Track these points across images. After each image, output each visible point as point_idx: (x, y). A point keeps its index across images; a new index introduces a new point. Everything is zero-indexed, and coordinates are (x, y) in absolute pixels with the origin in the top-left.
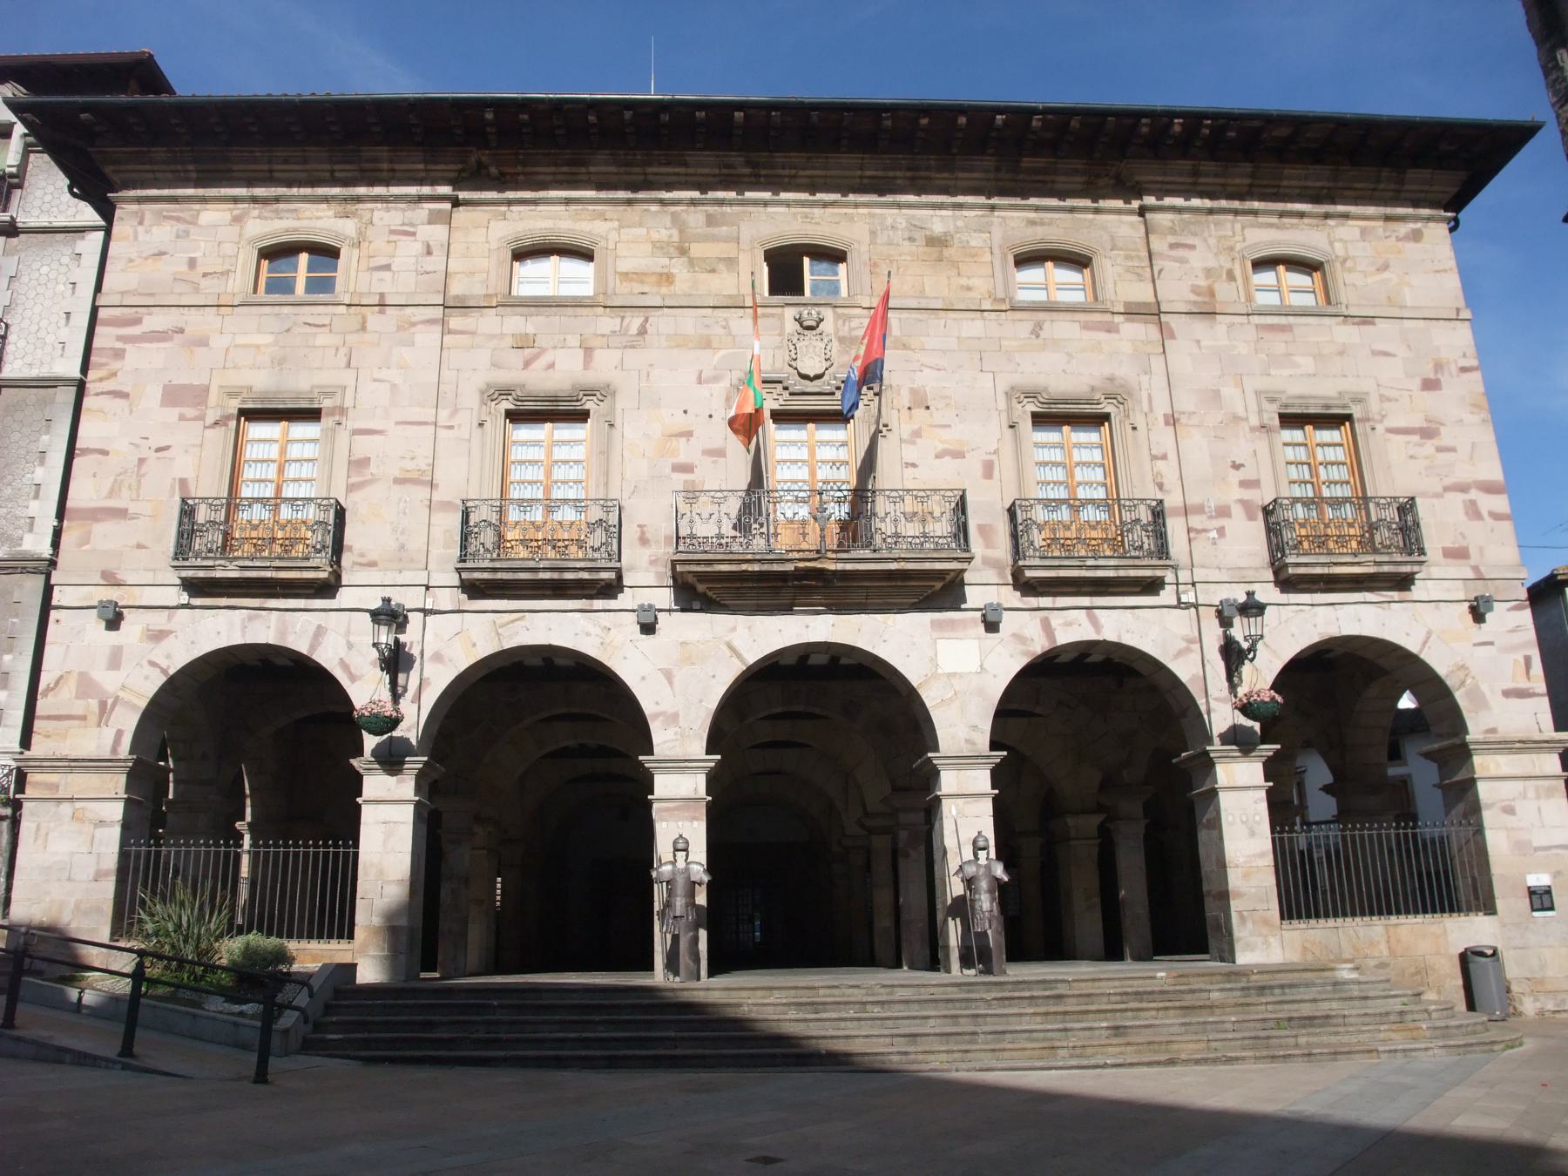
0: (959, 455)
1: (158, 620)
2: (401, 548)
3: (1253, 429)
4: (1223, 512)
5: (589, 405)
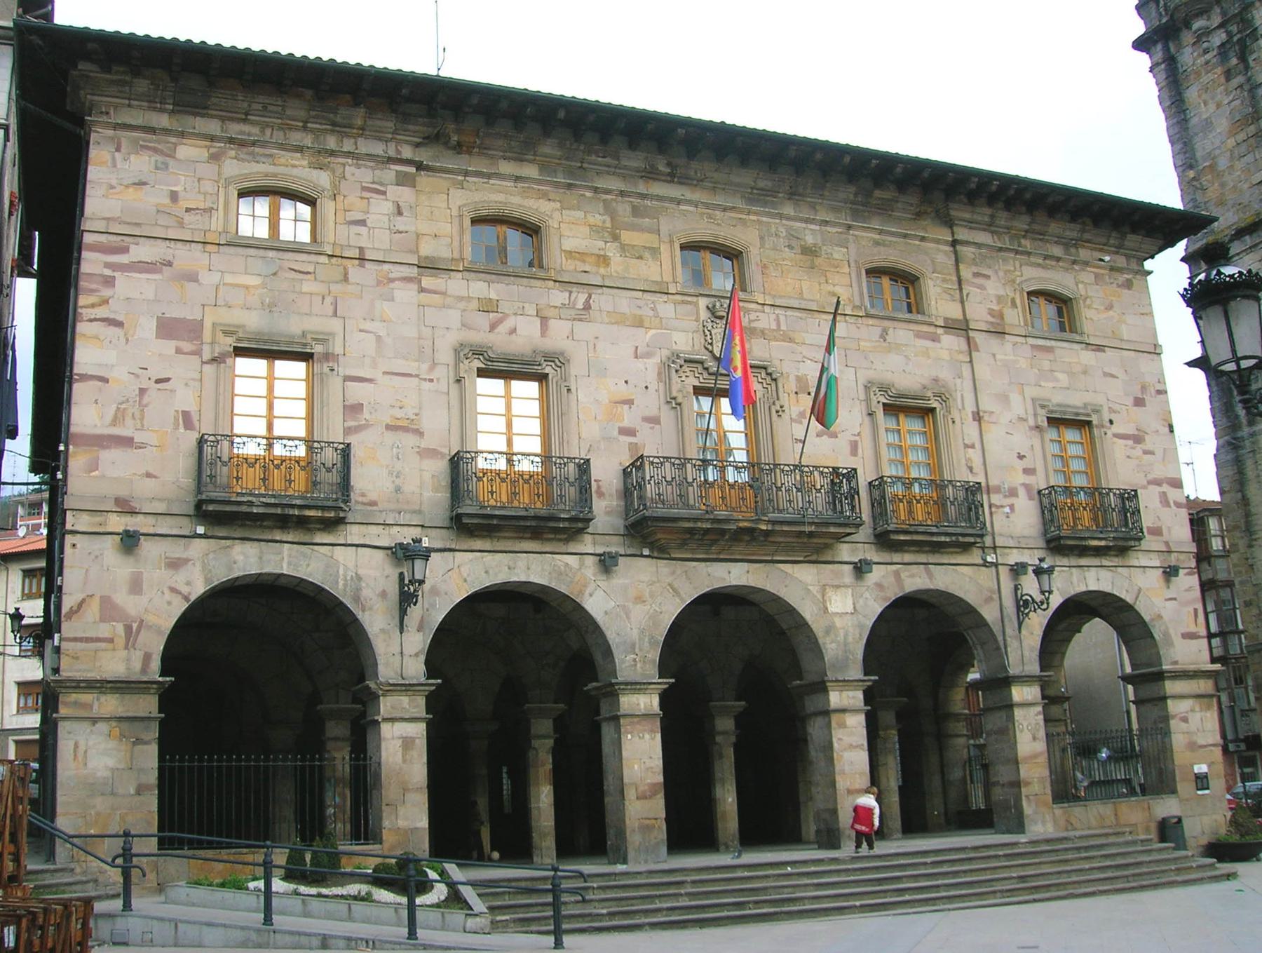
1: (175, 550)
2: (395, 478)
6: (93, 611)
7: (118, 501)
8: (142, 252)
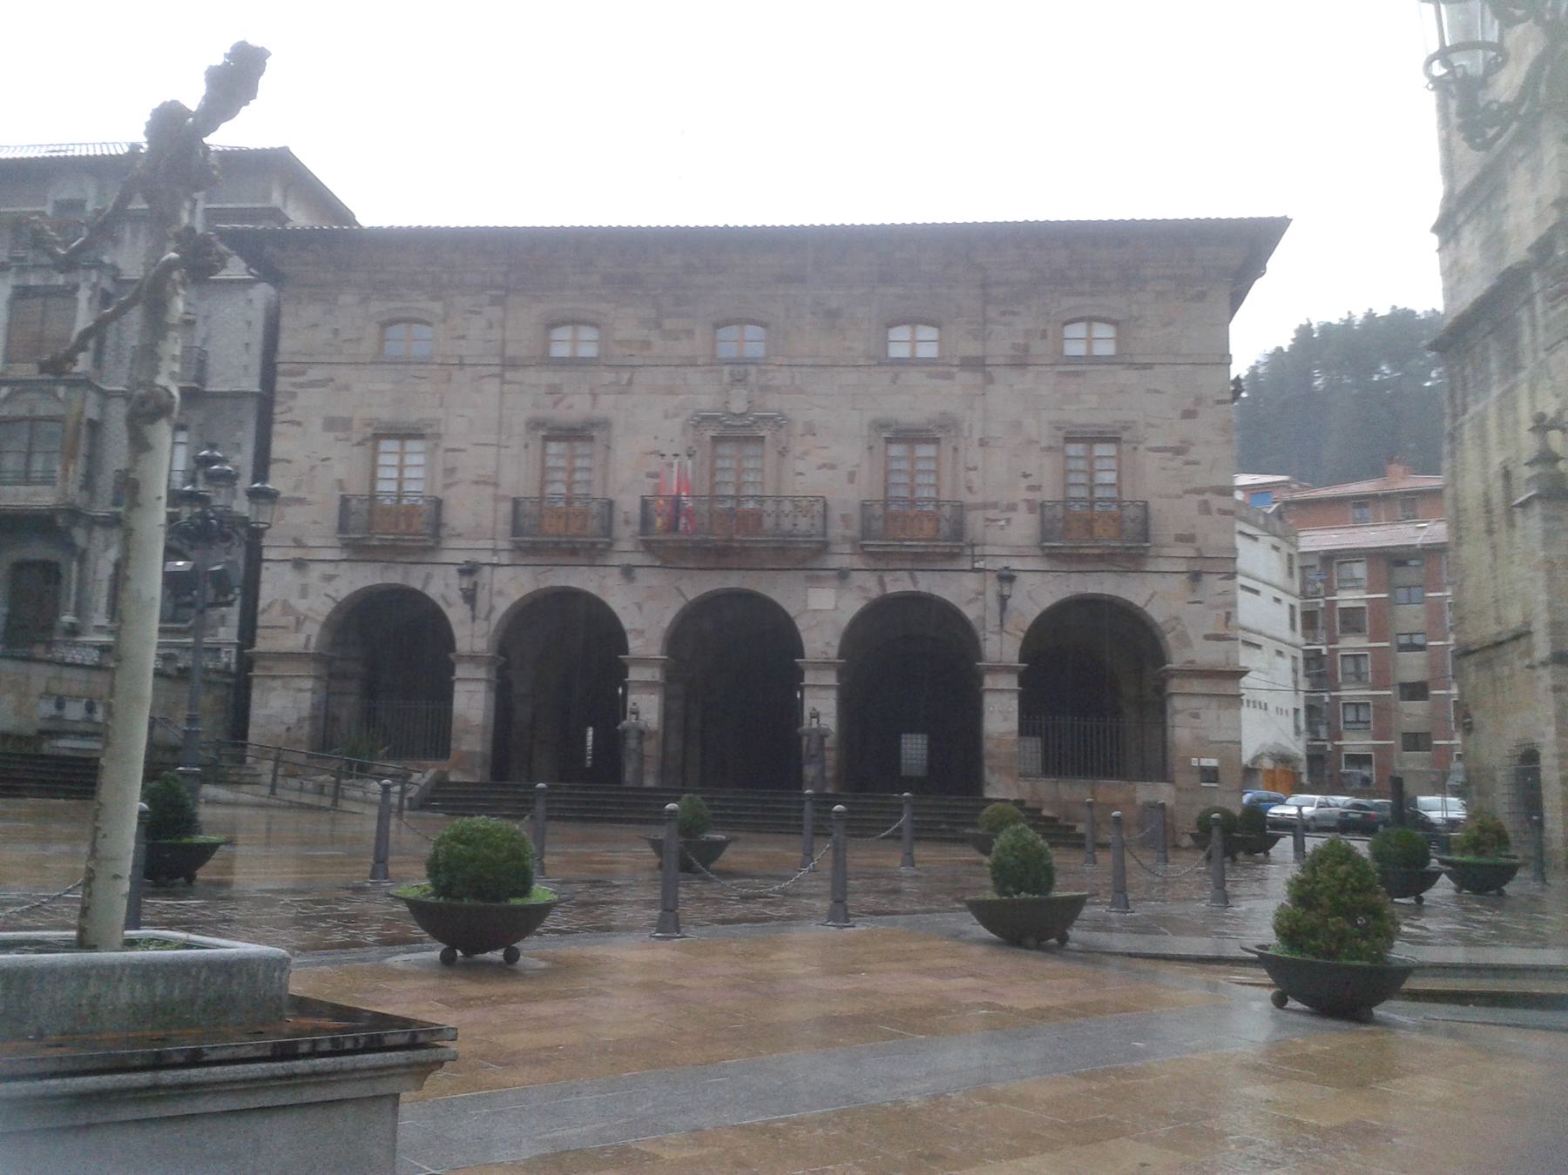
0: (832, 467)
1: (329, 569)
2: (475, 517)
3: (1042, 449)
4: (1012, 507)
5: (595, 434)
6: (277, 609)
7: (295, 540)
8: (314, 374)
